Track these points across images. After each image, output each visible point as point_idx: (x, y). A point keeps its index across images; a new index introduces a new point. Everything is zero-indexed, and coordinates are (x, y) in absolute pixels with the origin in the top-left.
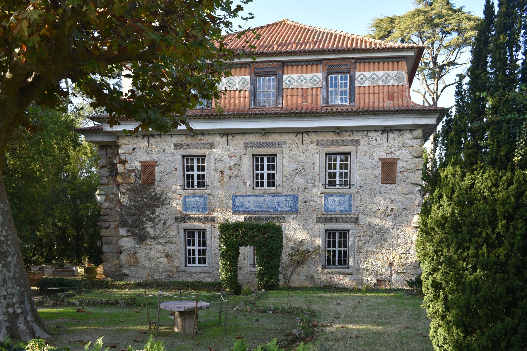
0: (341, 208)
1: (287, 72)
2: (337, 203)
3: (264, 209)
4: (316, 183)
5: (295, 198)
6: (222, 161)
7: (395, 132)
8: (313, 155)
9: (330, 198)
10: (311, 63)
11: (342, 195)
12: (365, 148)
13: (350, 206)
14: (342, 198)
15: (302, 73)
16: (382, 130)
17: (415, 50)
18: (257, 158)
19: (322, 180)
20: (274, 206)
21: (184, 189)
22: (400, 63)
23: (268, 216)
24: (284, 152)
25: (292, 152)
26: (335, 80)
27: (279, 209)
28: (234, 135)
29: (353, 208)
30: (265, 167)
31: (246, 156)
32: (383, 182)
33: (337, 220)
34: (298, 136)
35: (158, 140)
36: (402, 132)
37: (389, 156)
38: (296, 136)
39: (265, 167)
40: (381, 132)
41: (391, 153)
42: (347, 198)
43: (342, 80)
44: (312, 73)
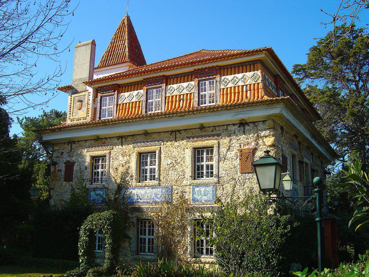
1: (184, 80)
2: (202, 192)
3: (145, 201)
4: (186, 176)
6: (117, 159)
7: (250, 124)
8: (184, 150)
9: (197, 189)
10: (187, 74)
11: (207, 185)
14: (207, 188)
15: (254, 71)
16: (239, 124)
17: (264, 52)
18: (197, 153)
19: (189, 172)
20: (153, 197)
21: (195, 179)
22: (256, 65)
23: (148, 206)
24: (162, 148)
25: (167, 149)
26: (205, 85)
27: (157, 200)
28: (126, 137)
31: (134, 154)
32: (65, 181)
34: (172, 134)
35: (77, 145)
36: (256, 124)
38: (171, 134)
40: (238, 125)
41: (248, 144)
43: (157, 93)
44: (128, 92)
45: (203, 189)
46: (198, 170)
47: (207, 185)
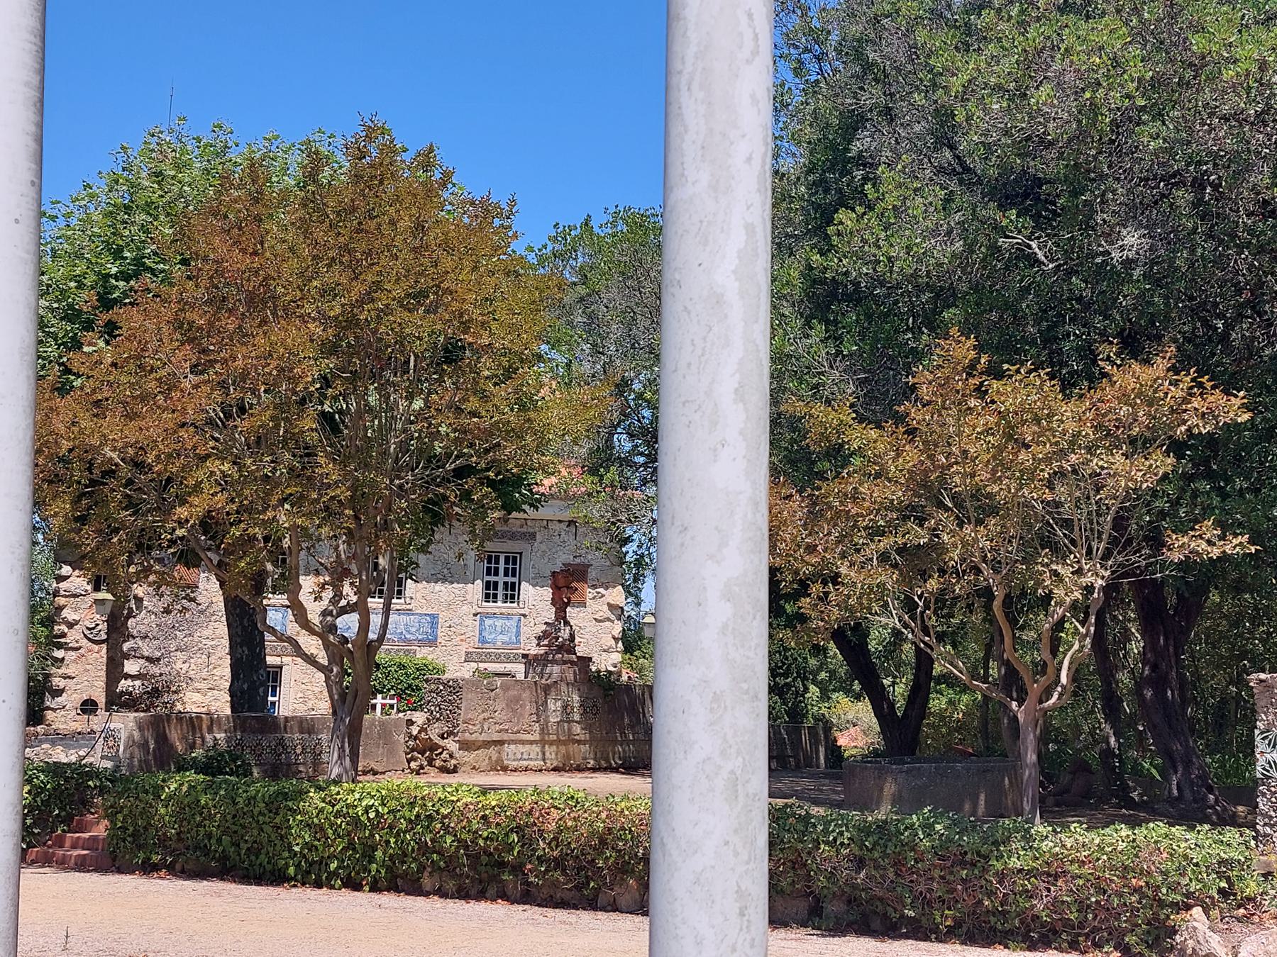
0: (506, 638)
2: (499, 629)
5: (434, 619)
9: (488, 622)
11: (508, 616)
12: (543, 547)
13: (518, 634)
29: (522, 638)
30: (501, 572)
33: (497, 659)
37: (578, 560)
39: (501, 572)
42: (513, 623)
45: (499, 623)
46: (514, 570)
47: (508, 616)
